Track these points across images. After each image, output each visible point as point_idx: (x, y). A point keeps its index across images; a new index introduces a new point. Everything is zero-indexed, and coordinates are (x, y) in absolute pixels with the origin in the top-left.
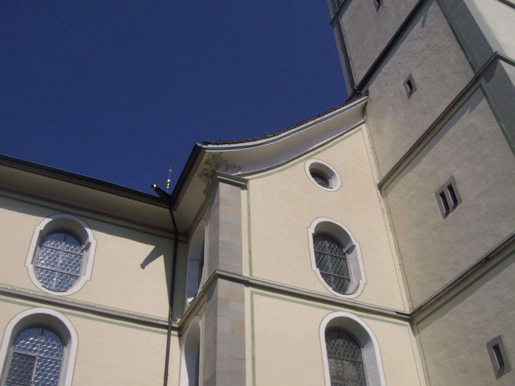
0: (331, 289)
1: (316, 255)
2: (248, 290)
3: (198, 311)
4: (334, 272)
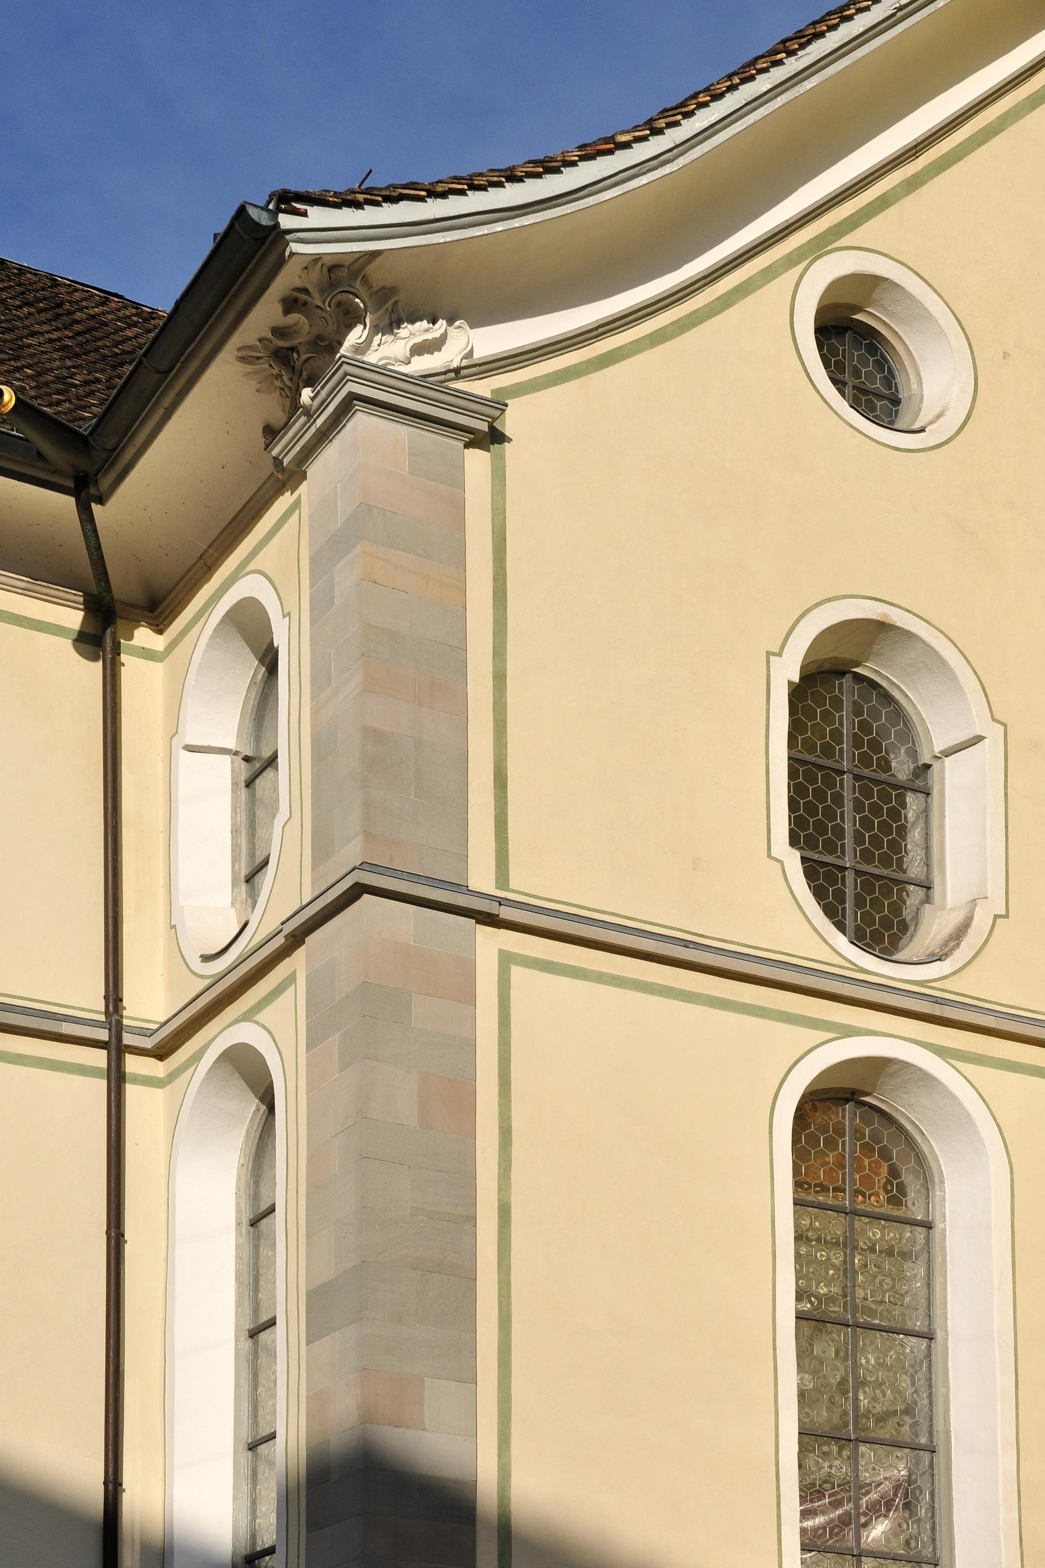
0: (841, 942)
1: (792, 774)
2: (490, 942)
3: (259, 1007)
4: (867, 857)
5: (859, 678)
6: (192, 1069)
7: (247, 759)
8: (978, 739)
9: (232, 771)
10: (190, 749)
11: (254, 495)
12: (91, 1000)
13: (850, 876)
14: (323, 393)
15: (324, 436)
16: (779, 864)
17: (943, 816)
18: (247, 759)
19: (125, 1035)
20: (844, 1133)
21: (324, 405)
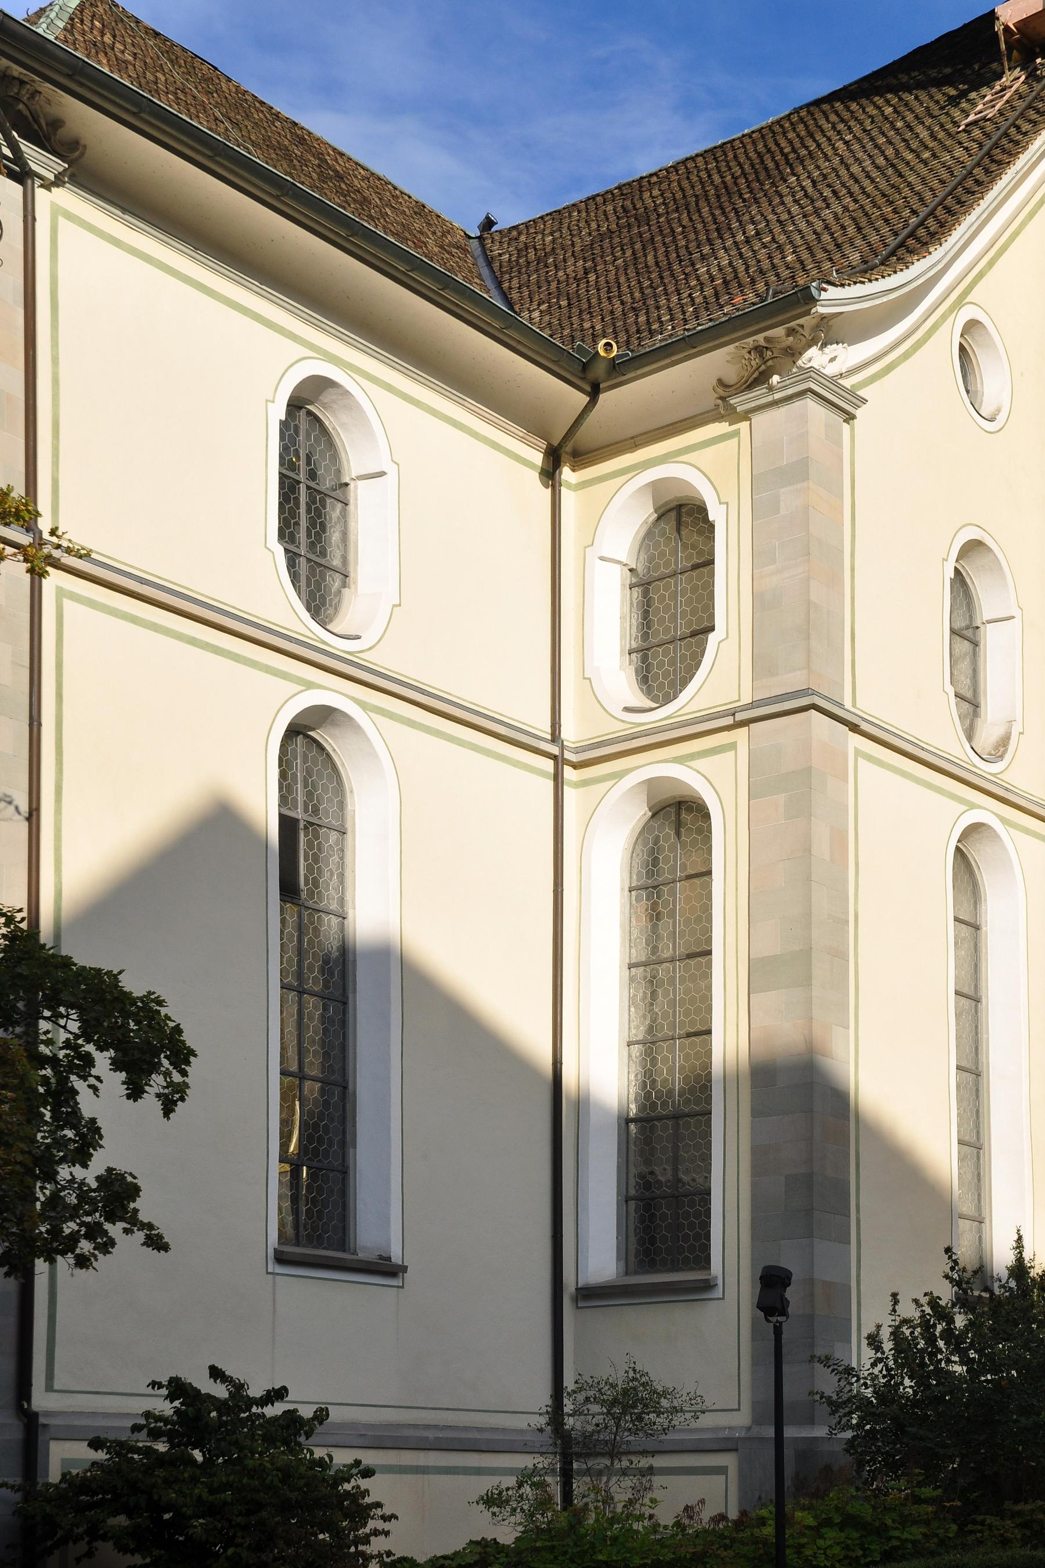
6: (614, 781)
10: (602, 559)
11: (695, 416)
14: (788, 382)
15: (775, 403)
17: (985, 662)
21: (785, 388)
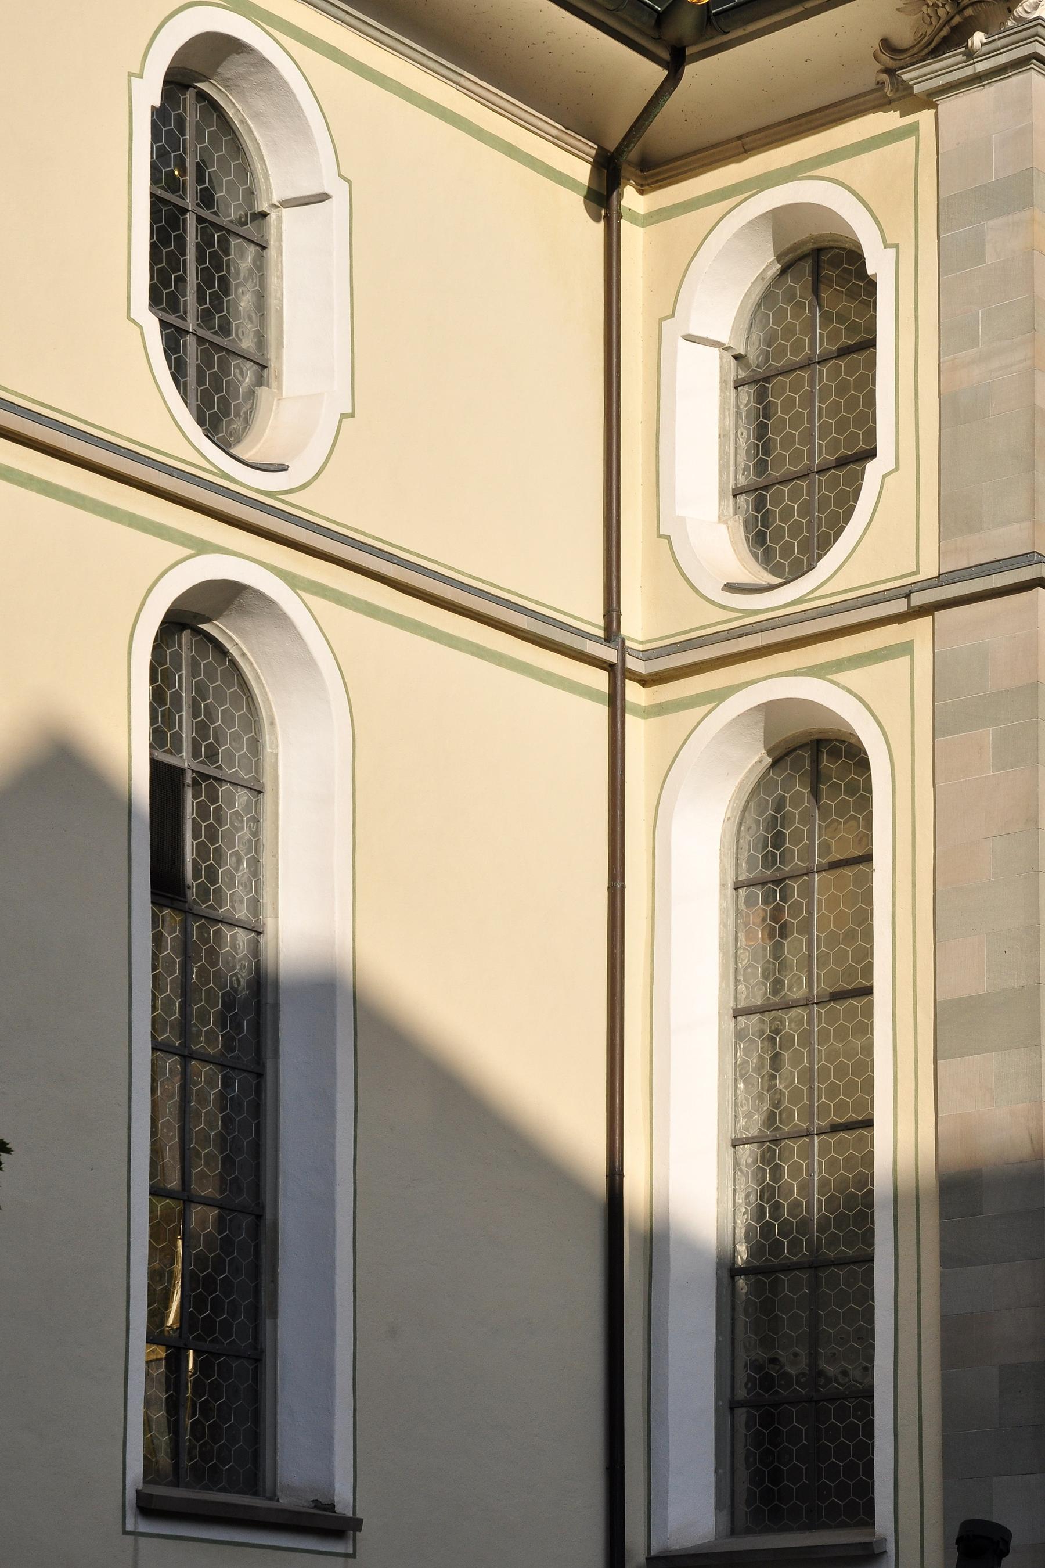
5: (202, 96)
7: (737, 357)
8: (322, 198)
9: (721, 367)
12: (589, 613)
13: (190, 340)
14: (999, 43)
16: (132, 316)
18: (737, 357)
19: (628, 657)
20: (180, 666)
